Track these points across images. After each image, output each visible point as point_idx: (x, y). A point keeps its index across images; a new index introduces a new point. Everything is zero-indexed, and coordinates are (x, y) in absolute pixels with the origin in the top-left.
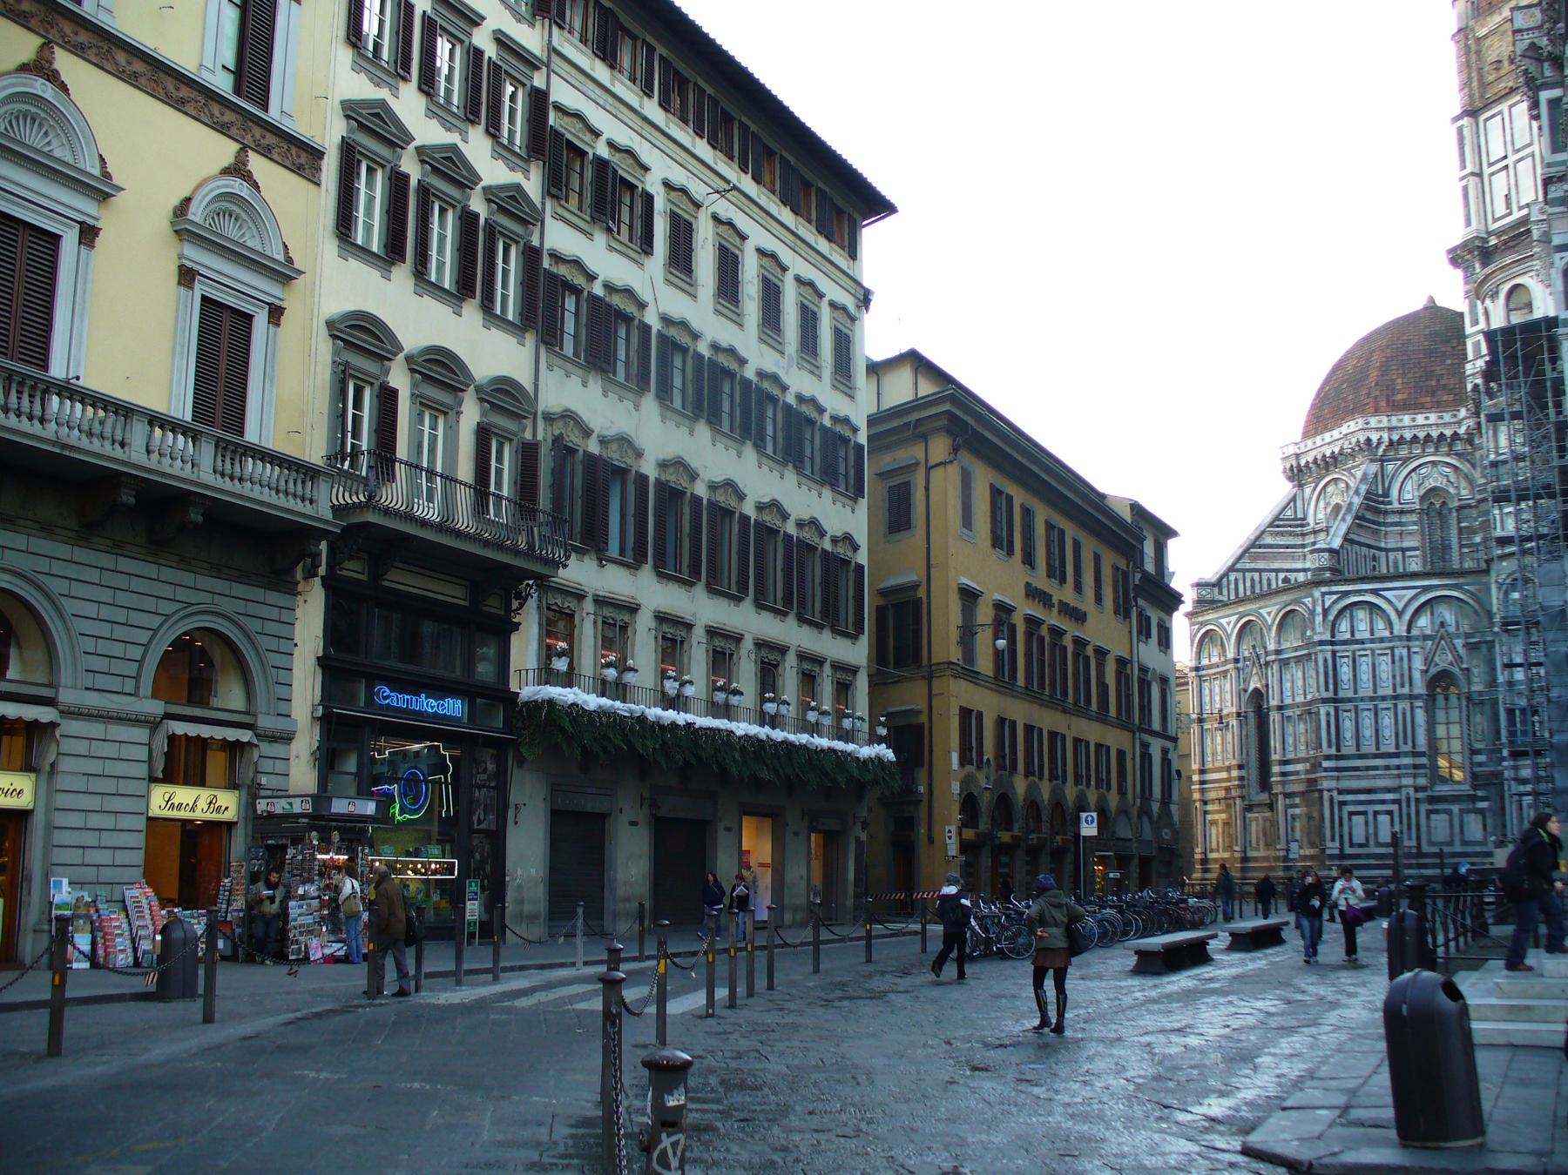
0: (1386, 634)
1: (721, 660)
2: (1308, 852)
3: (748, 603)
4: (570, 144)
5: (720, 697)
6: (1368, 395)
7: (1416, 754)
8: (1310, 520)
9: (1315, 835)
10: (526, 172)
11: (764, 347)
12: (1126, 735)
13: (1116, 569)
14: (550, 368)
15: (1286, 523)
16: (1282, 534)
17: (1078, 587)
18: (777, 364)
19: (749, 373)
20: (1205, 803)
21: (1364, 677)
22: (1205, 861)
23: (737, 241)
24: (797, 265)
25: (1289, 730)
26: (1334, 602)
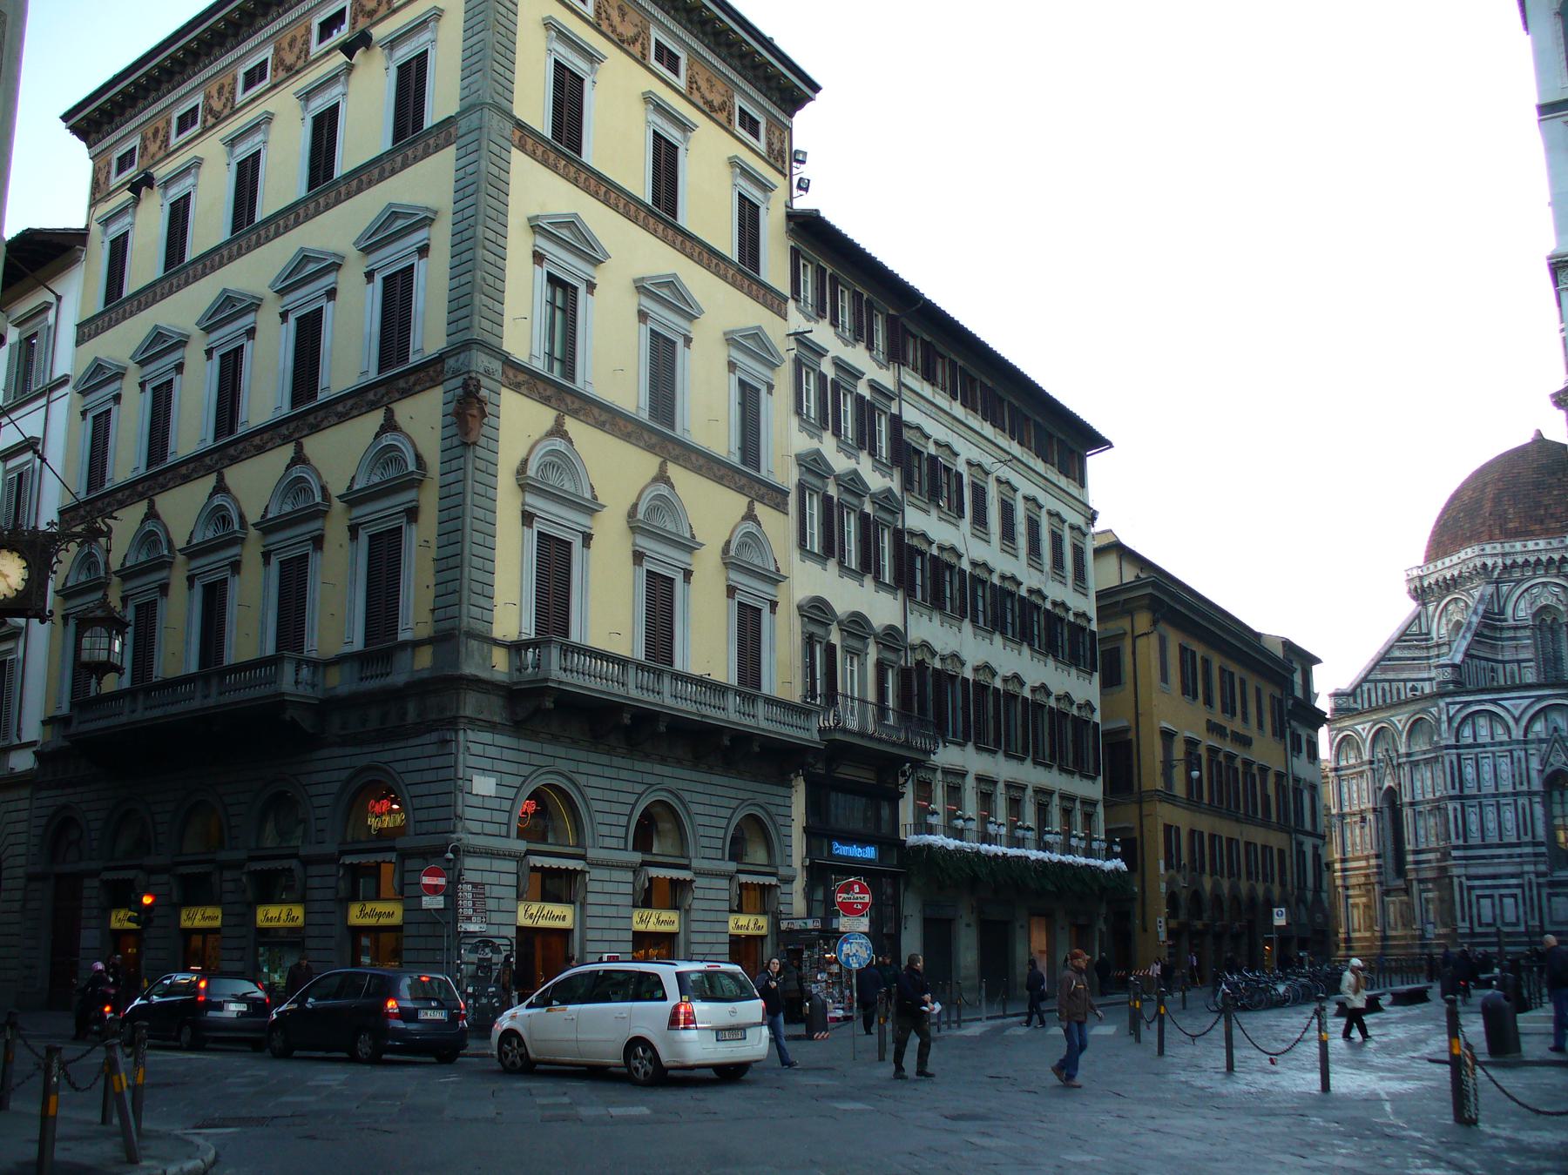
0: (1505, 738)
2: (1442, 931)
3: (1029, 762)
6: (1483, 524)
7: (1536, 844)
8: (1434, 634)
9: (1447, 916)
12: (1285, 836)
13: (1273, 697)
15: (1411, 638)
16: (1409, 648)
17: (1245, 718)
20: (1347, 888)
21: (1487, 777)
22: (1348, 940)
25: (1421, 823)
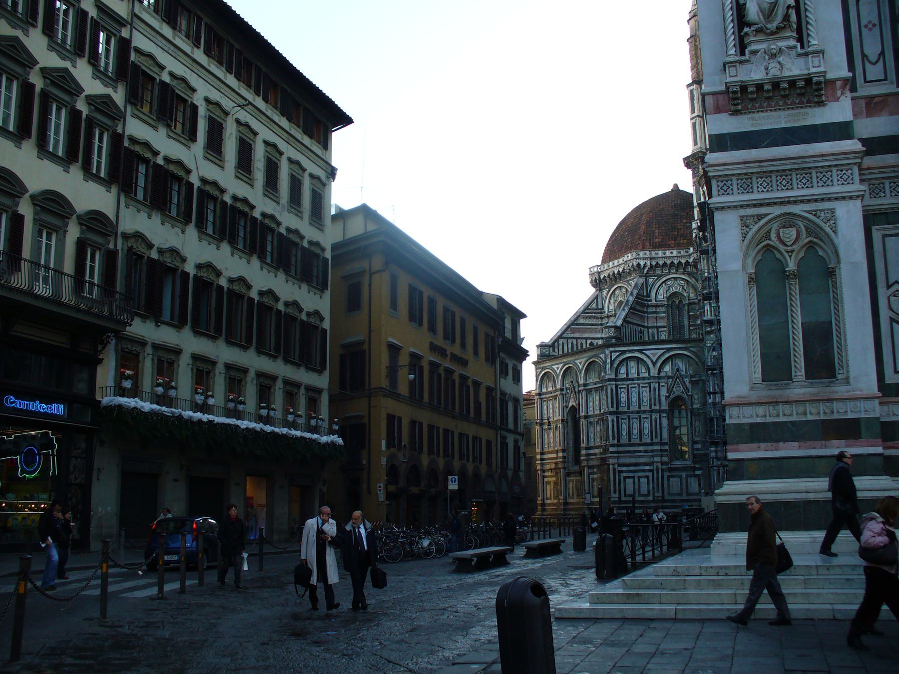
0: (647, 375)
1: (290, 397)
4: (144, 72)
5: (231, 405)
7: (661, 444)
8: (606, 309)
10: (115, 89)
11: (267, 199)
13: (487, 335)
14: (127, 206)
15: (590, 311)
16: (590, 317)
17: (463, 345)
18: (274, 209)
19: (257, 214)
20: (544, 471)
21: (634, 400)
22: (543, 505)
23: (251, 136)
24: (289, 151)
25: (591, 430)
26: (617, 357)
